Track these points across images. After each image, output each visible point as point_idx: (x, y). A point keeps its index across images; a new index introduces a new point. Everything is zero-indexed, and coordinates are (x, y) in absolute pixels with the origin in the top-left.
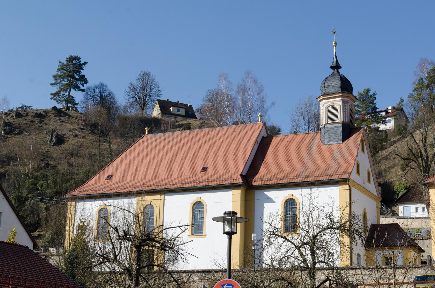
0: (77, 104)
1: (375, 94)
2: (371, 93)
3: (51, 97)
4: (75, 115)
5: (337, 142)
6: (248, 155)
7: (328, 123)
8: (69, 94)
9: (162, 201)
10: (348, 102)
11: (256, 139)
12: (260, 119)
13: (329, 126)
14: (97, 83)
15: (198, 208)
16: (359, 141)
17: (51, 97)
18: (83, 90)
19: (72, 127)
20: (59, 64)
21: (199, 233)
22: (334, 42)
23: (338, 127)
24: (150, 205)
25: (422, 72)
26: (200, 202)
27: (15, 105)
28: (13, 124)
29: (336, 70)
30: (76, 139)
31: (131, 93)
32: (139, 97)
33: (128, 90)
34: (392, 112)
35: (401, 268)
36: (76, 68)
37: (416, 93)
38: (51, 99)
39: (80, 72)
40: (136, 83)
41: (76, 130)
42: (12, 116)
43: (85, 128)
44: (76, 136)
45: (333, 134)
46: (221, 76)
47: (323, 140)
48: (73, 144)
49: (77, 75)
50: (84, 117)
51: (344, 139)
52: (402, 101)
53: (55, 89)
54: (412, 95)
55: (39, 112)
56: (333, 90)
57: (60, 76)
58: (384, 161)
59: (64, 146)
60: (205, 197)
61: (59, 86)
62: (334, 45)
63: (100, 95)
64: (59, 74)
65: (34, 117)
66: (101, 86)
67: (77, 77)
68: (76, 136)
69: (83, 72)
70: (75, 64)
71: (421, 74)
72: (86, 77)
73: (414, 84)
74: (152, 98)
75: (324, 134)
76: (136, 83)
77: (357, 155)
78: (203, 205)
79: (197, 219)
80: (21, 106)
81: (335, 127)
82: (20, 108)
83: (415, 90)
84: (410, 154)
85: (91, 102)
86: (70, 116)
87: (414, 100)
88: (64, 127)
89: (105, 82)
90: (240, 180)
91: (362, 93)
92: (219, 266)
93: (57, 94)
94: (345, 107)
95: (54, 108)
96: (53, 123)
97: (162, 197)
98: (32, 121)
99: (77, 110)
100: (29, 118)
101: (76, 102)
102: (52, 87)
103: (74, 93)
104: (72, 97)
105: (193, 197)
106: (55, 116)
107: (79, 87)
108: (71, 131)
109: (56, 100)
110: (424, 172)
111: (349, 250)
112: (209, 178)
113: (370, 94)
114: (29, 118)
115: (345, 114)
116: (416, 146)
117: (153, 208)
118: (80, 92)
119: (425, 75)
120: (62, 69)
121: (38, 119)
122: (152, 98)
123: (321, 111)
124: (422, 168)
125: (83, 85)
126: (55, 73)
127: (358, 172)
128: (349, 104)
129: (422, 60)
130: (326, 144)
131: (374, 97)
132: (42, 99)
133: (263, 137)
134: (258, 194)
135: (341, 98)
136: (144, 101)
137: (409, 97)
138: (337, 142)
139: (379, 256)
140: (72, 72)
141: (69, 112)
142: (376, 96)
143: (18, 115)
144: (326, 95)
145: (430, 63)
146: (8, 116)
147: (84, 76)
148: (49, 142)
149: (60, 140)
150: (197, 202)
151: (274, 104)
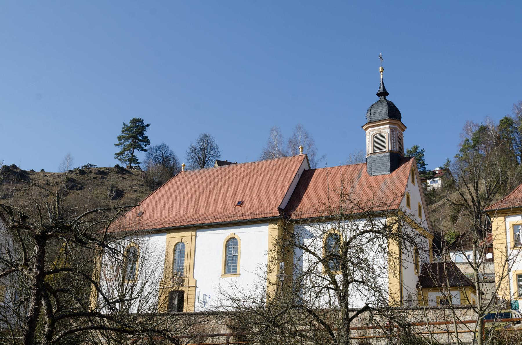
0: (139, 163)
1: (423, 151)
2: (419, 150)
3: (115, 156)
4: (137, 173)
5: (386, 173)
6: (288, 188)
7: (374, 153)
8: (132, 154)
9: (194, 238)
10: (396, 130)
11: (296, 171)
12: (302, 151)
13: (375, 155)
14: (159, 144)
15: (231, 244)
16: (409, 171)
17: (115, 156)
18: (146, 151)
19: (132, 183)
20: (123, 126)
21: (233, 272)
22: (380, 68)
23: (385, 156)
24: (181, 242)
25: (467, 134)
26: (234, 238)
27: (78, 163)
28: (75, 180)
29: (383, 97)
30: (135, 194)
31: (192, 154)
32: (199, 158)
33: (189, 151)
34: (439, 173)
35: (460, 308)
36: (139, 129)
37: (463, 153)
38: (115, 158)
39: (143, 134)
40: (196, 145)
41: (136, 186)
42: (76, 173)
43: (145, 184)
44: (136, 191)
45: (380, 164)
46: (272, 130)
47: (369, 170)
48: (131, 199)
49: (140, 136)
50: (146, 175)
51: (393, 169)
52: (449, 161)
53: (119, 150)
54: (458, 155)
55: (101, 170)
56: (379, 117)
57: (124, 137)
58: (434, 213)
59: (123, 200)
60: (240, 232)
61: (123, 146)
62: (380, 70)
63: (317, 300)
64: (123, 135)
65: (97, 174)
66: (162, 148)
67: (140, 138)
68: (136, 191)
69: (146, 134)
70: (138, 126)
71: (467, 136)
72: (149, 138)
73: (460, 145)
74: (211, 158)
75: (370, 164)
76: (196, 145)
77: (407, 186)
78: (237, 242)
79: (231, 257)
80: (86, 165)
81: (382, 156)
82: (85, 166)
83: (461, 151)
84: (461, 200)
85: (152, 162)
86: (133, 174)
87: (460, 160)
88: (125, 184)
89: (166, 143)
90: (277, 213)
91: (411, 150)
92: (227, 295)
93: (121, 154)
94: (393, 134)
95: (117, 166)
96: (113, 179)
97: (194, 233)
98: (94, 178)
99: (139, 168)
100: (92, 175)
101: (139, 161)
102: (117, 147)
103: (137, 153)
104: (135, 156)
105: (225, 234)
106: (118, 173)
107: (142, 148)
108: (131, 186)
109: (120, 160)
110: (476, 218)
111: (397, 262)
112: (245, 212)
113: (418, 151)
114: (92, 175)
115: (393, 142)
116: (468, 191)
117: (184, 246)
118: (142, 152)
119: (470, 136)
120: (126, 130)
121: (100, 176)
122: (211, 158)
123: (367, 140)
124: (474, 214)
125: (146, 146)
126: (120, 134)
127: (408, 204)
128: (397, 132)
129: (467, 122)
130: (373, 174)
131: (422, 153)
132: (106, 157)
133: (305, 170)
134: (296, 229)
135: (388, 126)
136: (204, 161)
137: (456, 157)
138: (384, 173)
139: (434, 296)
140: (136, 133)
141: (132, 170)
142: (424, 153)
143: (82, 172)
144: (373, 122)
145: (475, 126)
146: (72, 173)
147: (146, 137)
148: (108, 197)
149: (119, 194)
150: (231, 238)
151: (324, 157)
